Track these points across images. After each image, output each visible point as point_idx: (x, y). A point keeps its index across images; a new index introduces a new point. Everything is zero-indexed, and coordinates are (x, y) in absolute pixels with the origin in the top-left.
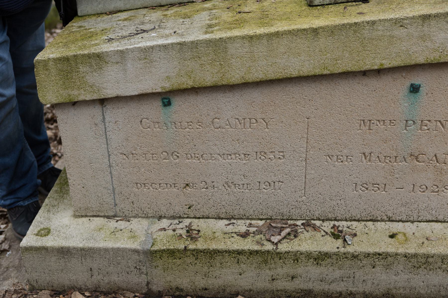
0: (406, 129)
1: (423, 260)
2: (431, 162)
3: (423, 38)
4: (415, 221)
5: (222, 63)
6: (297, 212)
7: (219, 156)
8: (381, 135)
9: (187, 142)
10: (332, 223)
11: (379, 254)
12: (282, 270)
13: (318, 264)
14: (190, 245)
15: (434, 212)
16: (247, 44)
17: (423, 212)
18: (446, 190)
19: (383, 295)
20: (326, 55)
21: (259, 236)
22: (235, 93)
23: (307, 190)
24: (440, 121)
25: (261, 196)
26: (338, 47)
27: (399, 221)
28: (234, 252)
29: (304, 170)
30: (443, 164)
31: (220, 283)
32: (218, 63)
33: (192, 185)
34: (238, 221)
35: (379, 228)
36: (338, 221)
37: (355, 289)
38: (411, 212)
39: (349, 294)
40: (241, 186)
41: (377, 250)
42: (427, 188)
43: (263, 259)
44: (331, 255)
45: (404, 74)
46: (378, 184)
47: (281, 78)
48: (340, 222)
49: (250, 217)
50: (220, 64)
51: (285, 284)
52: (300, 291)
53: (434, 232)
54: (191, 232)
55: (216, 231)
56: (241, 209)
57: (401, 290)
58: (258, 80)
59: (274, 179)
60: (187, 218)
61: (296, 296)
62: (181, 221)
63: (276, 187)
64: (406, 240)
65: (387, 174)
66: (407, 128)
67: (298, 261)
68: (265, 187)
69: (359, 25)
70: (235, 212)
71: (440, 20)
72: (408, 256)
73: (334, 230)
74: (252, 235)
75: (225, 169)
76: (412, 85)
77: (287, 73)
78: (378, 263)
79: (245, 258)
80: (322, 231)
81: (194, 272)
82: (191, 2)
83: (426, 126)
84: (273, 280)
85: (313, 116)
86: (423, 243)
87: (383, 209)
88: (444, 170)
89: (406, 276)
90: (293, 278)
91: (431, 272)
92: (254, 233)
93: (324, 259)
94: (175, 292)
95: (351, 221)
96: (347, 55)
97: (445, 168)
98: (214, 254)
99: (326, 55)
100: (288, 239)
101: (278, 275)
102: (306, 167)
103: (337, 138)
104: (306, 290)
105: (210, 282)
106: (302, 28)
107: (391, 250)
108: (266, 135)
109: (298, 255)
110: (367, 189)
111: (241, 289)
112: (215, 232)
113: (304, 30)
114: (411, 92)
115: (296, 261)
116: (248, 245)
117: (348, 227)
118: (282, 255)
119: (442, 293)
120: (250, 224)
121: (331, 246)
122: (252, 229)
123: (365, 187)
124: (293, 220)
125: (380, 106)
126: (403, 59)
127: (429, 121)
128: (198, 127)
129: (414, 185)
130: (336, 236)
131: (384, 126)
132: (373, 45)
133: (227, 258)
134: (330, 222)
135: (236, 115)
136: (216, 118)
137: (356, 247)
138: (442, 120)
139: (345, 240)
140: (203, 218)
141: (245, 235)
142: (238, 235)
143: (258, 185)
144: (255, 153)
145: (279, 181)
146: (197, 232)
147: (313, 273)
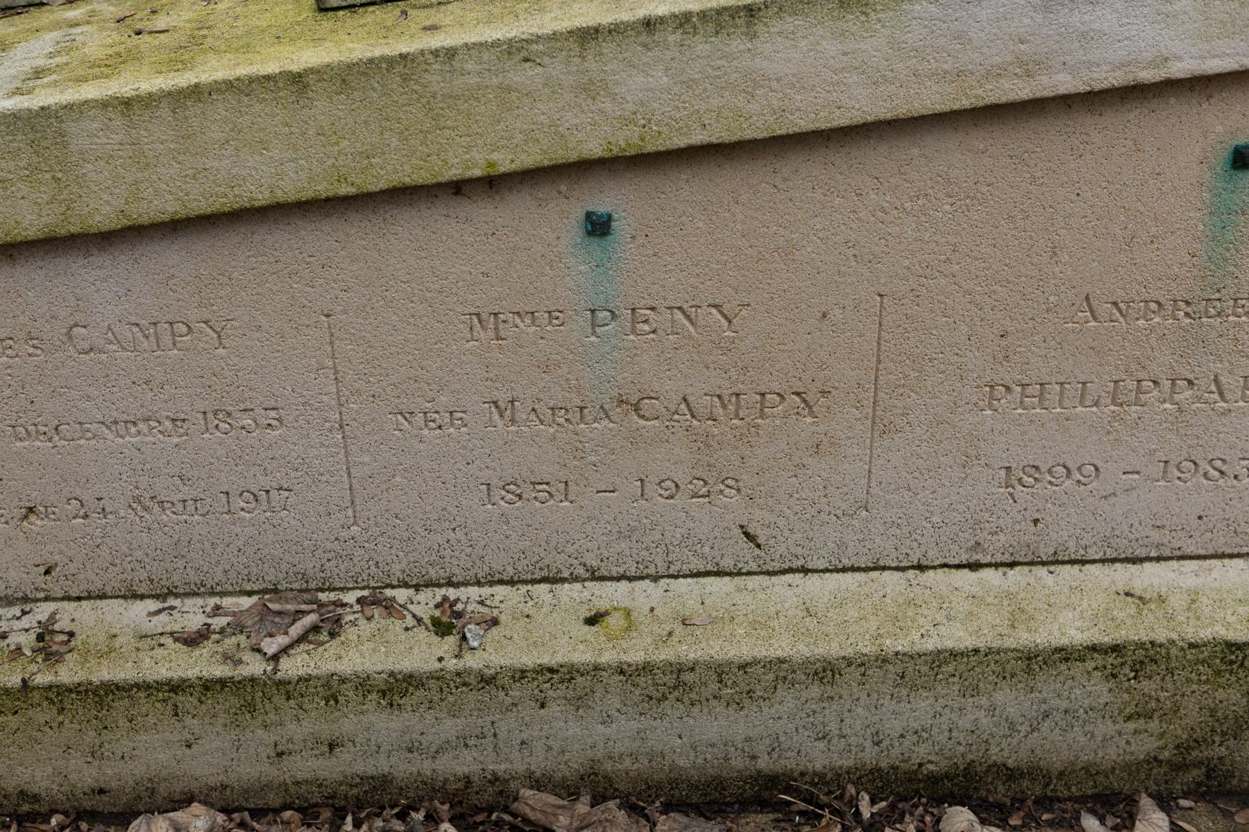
0: (594, 333)
1: (670, 680)
2: (676, 417)
3: (589, 89)
4: (663, 577)
5: (59, 175)
6: (342, 567)
7: (104, 429)
9: (7, 392)
10: (440, 592)
11: (551, 670)
12: (301, 727)
13: (392, 705)
14: (39, 676)
15: (707, 549)
16: (118, 122)
18: (727, 491)
19: (582, 779)
20: (337, 144)
21: (233, 638)
22: (117, 254)
23: (358, 508)
24: (679, 308)
25: (238, 530)
26: (365, 122)
27: (618, 579)
28: (159, 685)
29: (342, 456)
30: (710, 422)
31: (136, 772)
32: (48, 176)
33: (41, 509)
34: (186, 601)
35: (565, 599)
36: (457, 585)
37: (503, 767)
38: (647, 553)
39: (490, 781)
40: (180, 506)
41: (546, 660)
42: (677, 486)
43: (242, 702)
44: (424, 680)
45: (563, 188)
46: (547, 484)
47: (226, 209)
49: (219, 588)
50: (53, 177)
51: (313, 763)
52: (358, 780)
53: (706, 602)
54: (47, 638)
55: (118, 631)
56: (188, 569)
57: (627, 762)
58: (166, 218)
59: (266, 482)
60: (46, 599)
61: (350, 794)
62: (28, 609)
63: (273, 504)
64: (628, 629)
65: (564, 455)
66: (598, 330)
67: (337, 702)
68: (243, 504)
69: (413, 61)
70: (176, 578)
72: (629, 670)
73: (443, 612)
74: (217, 636)
75: (127, 461)
76: (589, 215)
77: (240, 196)
78: (551, 693)
79: (196, 702)
80: (409, 617)
81: (59, 746)
82: (37, 5)
83: (646, 321)
84: (280, 755)
85: (340, 308)
86: (670, 634)
87: (570, 549)
88: (714, 436)
89: (634, 725)
90: (332, 747)
91: (696, 710)
92: (222, 631)
93: (407, 691)
94: (18, 805)
95: (491, 584)
96: (394, 142)
98: (107, 694)
99: (337, 144)
100: (310, 642)
101: (290, 740)
102: (345, 447)
103: (415, 364)
104: (372, 778)
105: (109, 772)
106: (262, 73)
107: (582, 657)
108: (223, 364)
109: (335, 684)
110: (520, 496)
111: (196, 784)
112: (115, 636)
113: (268, 78)
114: (590, 233)
115: (332, 702)
116: (201, 664)
117: (481, 603)
118: (290, 688)
119: (733, 762)
120: (217, 607)
121: (422, 653)
122: (219, 622)
124: (334, 589)
126: (545, 147)
127: (653, 309)
128: (31, 350)
129: (642, 480)
130: (441, 628)
131: (534, 328)
132: (459, 112)
133: (144, 704)
134: (436, 589)
135: (130, 314)
136: (76, 325)
137: (491, 653)
138: (685, 306)
139: (464, 638)
140: (89, 598)
141: (193, 640)
142: (176, 640)
143: (224, 500)
144: (200, 416)
145: (281, 489)
146: (65, 638)
147: (383, 732)
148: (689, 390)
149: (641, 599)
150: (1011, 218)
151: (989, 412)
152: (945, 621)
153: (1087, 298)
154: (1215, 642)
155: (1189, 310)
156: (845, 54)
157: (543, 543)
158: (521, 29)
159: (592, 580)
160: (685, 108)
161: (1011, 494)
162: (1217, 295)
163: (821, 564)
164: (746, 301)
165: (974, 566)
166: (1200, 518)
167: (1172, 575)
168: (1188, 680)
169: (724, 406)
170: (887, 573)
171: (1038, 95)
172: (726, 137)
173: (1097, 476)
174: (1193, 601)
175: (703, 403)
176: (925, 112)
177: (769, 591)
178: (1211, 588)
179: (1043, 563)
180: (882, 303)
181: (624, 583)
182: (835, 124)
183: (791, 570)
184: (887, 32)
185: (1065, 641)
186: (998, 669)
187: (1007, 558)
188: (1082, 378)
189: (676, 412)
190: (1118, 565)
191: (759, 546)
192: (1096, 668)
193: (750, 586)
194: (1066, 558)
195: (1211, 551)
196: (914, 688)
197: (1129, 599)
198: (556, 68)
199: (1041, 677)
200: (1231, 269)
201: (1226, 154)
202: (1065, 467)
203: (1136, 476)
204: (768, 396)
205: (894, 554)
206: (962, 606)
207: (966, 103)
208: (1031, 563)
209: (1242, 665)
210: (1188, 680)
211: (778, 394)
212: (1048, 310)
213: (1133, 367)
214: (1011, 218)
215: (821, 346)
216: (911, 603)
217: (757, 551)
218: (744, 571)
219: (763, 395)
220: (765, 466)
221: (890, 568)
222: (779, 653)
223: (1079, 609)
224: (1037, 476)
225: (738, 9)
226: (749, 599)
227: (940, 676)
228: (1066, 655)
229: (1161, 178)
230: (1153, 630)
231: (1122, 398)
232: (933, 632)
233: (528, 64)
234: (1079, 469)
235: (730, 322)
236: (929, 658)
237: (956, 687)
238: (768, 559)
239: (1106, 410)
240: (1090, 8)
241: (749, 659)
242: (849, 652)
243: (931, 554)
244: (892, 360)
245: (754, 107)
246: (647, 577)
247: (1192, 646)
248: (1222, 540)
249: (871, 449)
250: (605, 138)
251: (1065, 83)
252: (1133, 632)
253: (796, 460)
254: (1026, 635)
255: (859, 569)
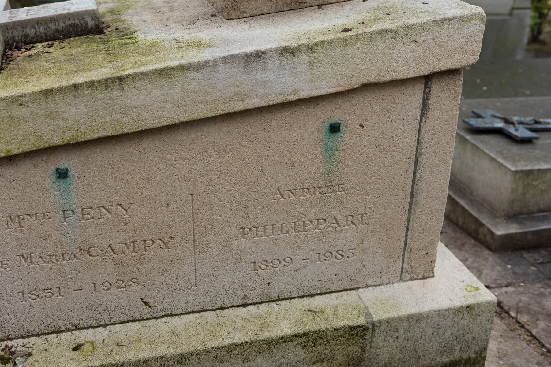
0: (65, 221)
2: (107, 254)
3: (50, 115)
4: (108, 325)
8: (37, 231)
15: (127, 311)
17: (114, 312)
18: (134, 284)
24: (103, 207)
27: (88, 328)
30: (122, 255)
36: (12, 339)
38: (100, 315)
42: (110, 284)
45: (44, 159)
46: (50, 289)
48: (14, 341)
64: (93, 351)
65: (57, 276)
71: (66, 94)
73: (5, 353)
76: (57, 170)
83: (88, 214)
86: (112, 351)
87: (64, 317)
88: (125, 261)
95: (28, 337)
97: (125, 259)
110: (38, 296)
114: (59, 177)
117: (24, 346)
123: (34, 295)
125: (26, 198)
126: (33, 142)
127: (91, 208)
129: (94, 283)
131: (37, 221)
138: (106, 206)
148: (111, 242)
149: (98, 336)
150: (243, 158)
151: (243, 240)
152: (233, 331)
153: (278, 189)
154: (345, 327)
155: (320, 191)
156: (163, 95)
157: (51, 316)
158: (18, 91)
159: (76, 330)
160: (95, 122)
161: (257, 273)
162: (331, 184)
163: (179, 312)
164: (133, 201)
165: (245, 305)
166: (336, 275)
167: (327, 300)
168: (336, 344)
169: (128, 248)
170: (208, 312)
171: (247, 108)
172: (115, 133)
173: (292, 262)
174: (336, 311)
175: (118, 247)
176: (200, 118)
177: (156, 326)
178: (343, 305)
179: (274, 301)
180: (192, 198)
181: (91, 330)
182: (162, 125)
183: (166, 316)
184: (180, 85)
185: (283, 334)
186: (257, 349)
187: (258, 300)
188: (281, 222)
189: (107, 252)
190: (305, 298)
191: (150, 307)
192: (298, 344)
193: (148, 325)
194: (283, 298)
195: (342, 289)
196: (221, 362)
197: (310, 312)
198: (35, 107)
199: (275, 350)
200: (335, 173)
201: (327, 127)
202: (278, 259)
203: (308, 261)
204: (147, 242)
205: (210, 304)
206: (240, 323)
207: (217, 113)
208: (269, 301)
209: (357, 335)
210: (336, 344)
211: (151, 240)
212: (263, 195)
213: (301, 216)
214: (243, 158)
215: (168, 218)
216: (218, 324)
217: (150, 309)
218: (145, 318)
219: (145, 241)
220: (149, 272)
221: (209, 310)
222: (161, 354)
223: (289, 319)
224: (267, 264)
225: (115, 78)
226: (147, 331)
227: (232, 355)
228: (284, 340)
229: (303, 138)
230: (319, 325)
231: (298, 229)
232: (228, 337)
233: (22, 106)
234: (284, 260)
235: (126, 211)
236: (227, 348)
237: (240, 359)
238: (155, 312)
239: (292, 234)
240: (264, 72)
241: (147, 358)
242: (192, 350)
243: (226, 302)
244: (199, 222)
245: (126, 120)
246: (101, 326)
247: (336, 330)
248: (346, 284)
249: (195, 260)
250: (61, 136)
251: (258, 103)
252: (311, 327)
253: (163, 268)
254: (267, 333)
255: (195, 312)
